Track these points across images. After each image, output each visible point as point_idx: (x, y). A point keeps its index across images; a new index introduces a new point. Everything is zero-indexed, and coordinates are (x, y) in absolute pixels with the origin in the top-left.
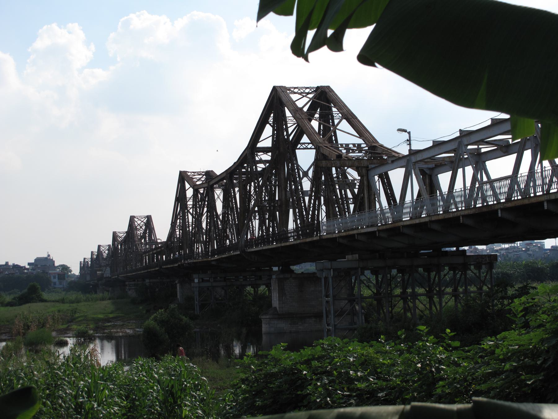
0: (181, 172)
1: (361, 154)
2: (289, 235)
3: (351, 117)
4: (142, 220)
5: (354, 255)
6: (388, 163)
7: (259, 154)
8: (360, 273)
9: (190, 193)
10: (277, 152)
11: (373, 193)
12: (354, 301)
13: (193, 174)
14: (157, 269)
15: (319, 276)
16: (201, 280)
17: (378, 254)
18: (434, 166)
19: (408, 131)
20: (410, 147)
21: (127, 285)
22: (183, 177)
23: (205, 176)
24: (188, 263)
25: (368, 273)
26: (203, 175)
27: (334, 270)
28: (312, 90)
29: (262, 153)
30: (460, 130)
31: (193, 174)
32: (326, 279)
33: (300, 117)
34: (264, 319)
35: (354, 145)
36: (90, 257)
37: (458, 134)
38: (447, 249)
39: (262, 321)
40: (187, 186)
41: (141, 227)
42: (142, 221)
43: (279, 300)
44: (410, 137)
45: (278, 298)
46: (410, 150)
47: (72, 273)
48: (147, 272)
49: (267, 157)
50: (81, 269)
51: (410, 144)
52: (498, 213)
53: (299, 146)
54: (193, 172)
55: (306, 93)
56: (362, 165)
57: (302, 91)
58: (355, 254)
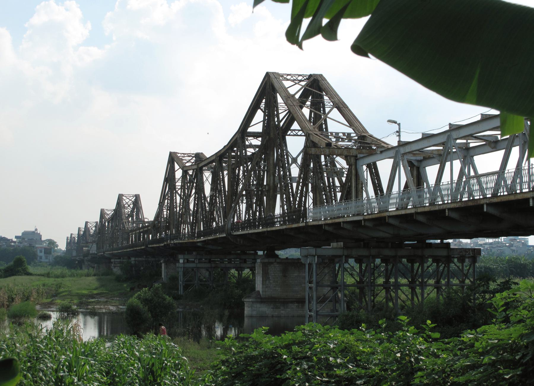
1: (350, 143)
2: (276, 220)
4: (130, 198)
5: (339, 243)
7: (249, 138)
8: (344, 261)
9: (179, 174)
10: (268, 137)
13: (183, 155)
14: (143, 247)
15: (303, 262)
16: (186, 261)
17: (362, 243)
19: (398, 123)
20: (400, 138)
22: (173, 158)
23: (194, 158)
25: (352, 261)
26: (193, 157)
29: (253, 138)
30: (450, 124)
31: (183, 155)
33: (292, 104)
37: (447, 128)
40: (177, 167)
41: (129, 206)
42: (130, 200)
43: (263, 284)
44: (399, 129)
45: (261, 282)
46: (399, 141)
47: (59, 248)
48: (133, 250)
49: (257, 142)
51: (399, 136)
53: (290, 132)
54: (183, 154)
56: (351, 155)
57: (295, 78)
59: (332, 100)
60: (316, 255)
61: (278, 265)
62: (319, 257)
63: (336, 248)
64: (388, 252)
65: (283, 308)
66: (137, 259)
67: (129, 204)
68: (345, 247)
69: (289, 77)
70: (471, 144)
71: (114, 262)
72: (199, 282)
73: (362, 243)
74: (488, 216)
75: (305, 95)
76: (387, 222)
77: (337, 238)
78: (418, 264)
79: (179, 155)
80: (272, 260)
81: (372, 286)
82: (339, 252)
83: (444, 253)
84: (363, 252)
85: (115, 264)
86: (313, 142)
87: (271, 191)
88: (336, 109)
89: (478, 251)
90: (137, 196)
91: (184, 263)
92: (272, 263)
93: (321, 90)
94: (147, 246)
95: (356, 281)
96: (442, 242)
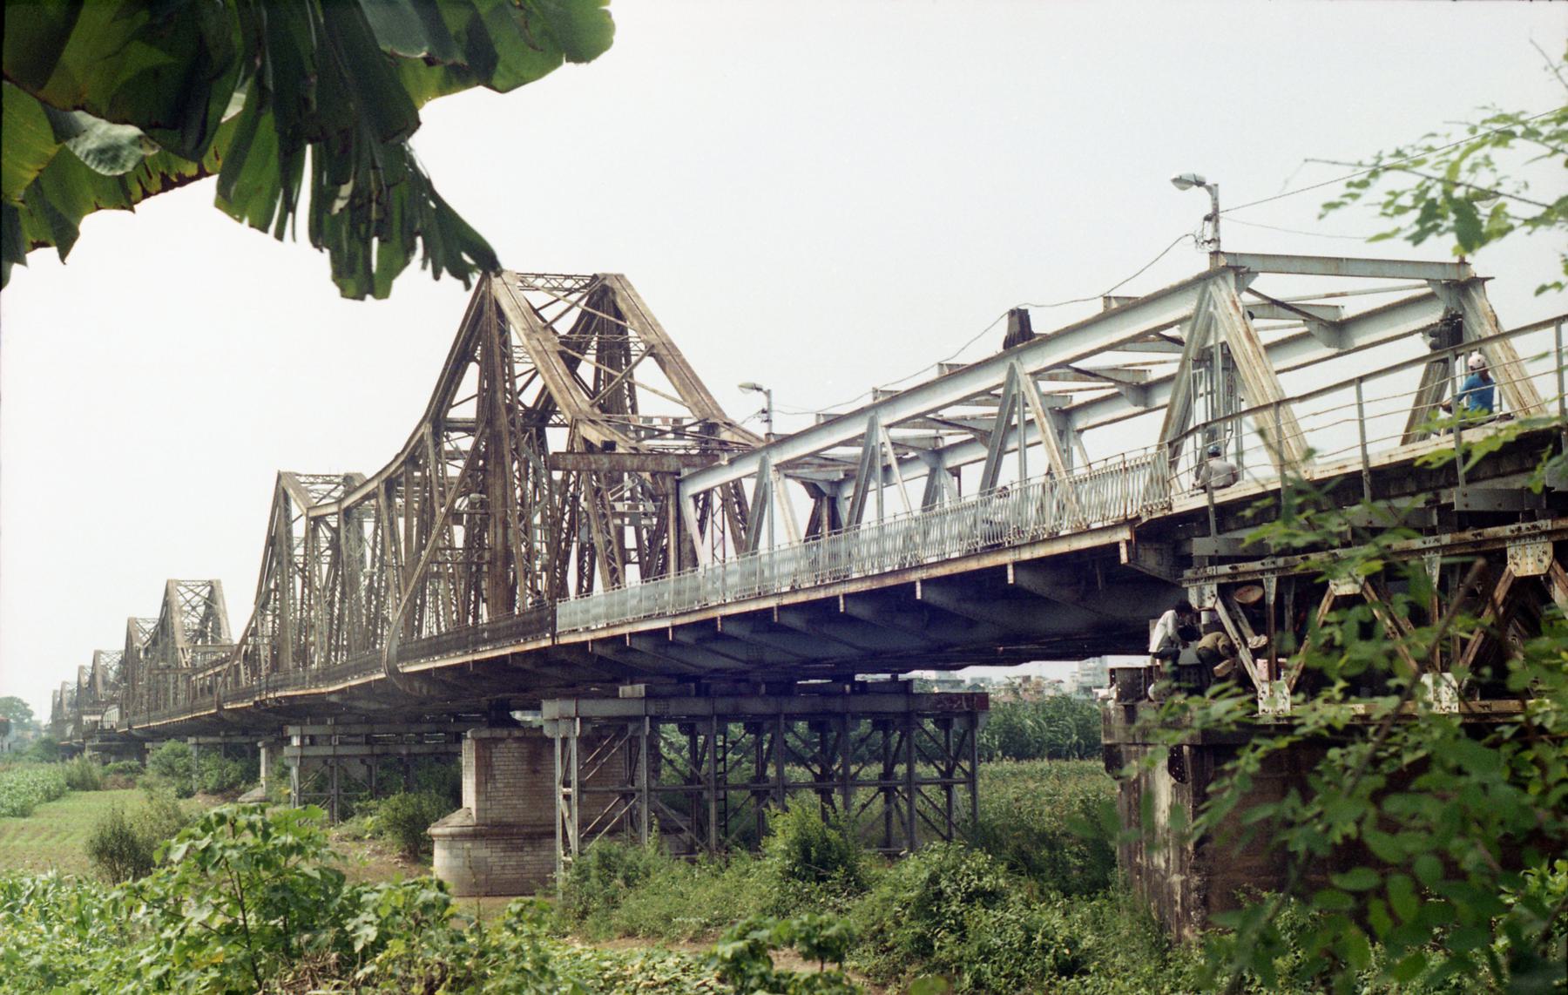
4: (197, 590)
6: (721, 466)
7: (454, 435)
8: (783, 726)
12: (633, 795)
13: (312, 479)
14: (213, 711)
16: (307, 741)
17: (693, 685)
18: (842, 476)
19: (765, 389)
20: (770, 427)
23: (341, 487)
25: (736, 729)
26: (339, 484)
28: (582, 283)
29: (464, 434)
30: (875, 391)
31: (312, 479)
32: (565, 741)
34: (438, 836)
35: (665, 420)
36: (75, 680)
40: (295, 511)
41: (194, 608)
42: (197, 594)
44: (769, 403)
47: (33, 718)
48: (192, 719)
49: (465, 443)
50: (57, 707)
51: (768, 421)
52: (914, 593)
55: (566, 290)
56: (666, 469)
57: (556, 285)
58: (639, 682)
59: (644, 337)
60: (577, 715)
61: (515, 745)
62: (584, 720)
63: (630, 698)
64: (755, 706)
65: (529, 849)
66: (202, 740)
67: (194, 604)
69: (540, 282)
72: (341, 791)
73: (693, 685)
75: (586, 323)
77: (632, 676)
78: (897, 735)
81: (718, 789)
82: (636, 709)
83: (897, 705)
84: (699, 706)
86: (586, 441)
87: (499, 563)
88: (652, 359)
90: (215, 584)
91: (302, 745)
92: (502, 740)
93: (619, 314)
94: (220, 708)
95: (815, 774)
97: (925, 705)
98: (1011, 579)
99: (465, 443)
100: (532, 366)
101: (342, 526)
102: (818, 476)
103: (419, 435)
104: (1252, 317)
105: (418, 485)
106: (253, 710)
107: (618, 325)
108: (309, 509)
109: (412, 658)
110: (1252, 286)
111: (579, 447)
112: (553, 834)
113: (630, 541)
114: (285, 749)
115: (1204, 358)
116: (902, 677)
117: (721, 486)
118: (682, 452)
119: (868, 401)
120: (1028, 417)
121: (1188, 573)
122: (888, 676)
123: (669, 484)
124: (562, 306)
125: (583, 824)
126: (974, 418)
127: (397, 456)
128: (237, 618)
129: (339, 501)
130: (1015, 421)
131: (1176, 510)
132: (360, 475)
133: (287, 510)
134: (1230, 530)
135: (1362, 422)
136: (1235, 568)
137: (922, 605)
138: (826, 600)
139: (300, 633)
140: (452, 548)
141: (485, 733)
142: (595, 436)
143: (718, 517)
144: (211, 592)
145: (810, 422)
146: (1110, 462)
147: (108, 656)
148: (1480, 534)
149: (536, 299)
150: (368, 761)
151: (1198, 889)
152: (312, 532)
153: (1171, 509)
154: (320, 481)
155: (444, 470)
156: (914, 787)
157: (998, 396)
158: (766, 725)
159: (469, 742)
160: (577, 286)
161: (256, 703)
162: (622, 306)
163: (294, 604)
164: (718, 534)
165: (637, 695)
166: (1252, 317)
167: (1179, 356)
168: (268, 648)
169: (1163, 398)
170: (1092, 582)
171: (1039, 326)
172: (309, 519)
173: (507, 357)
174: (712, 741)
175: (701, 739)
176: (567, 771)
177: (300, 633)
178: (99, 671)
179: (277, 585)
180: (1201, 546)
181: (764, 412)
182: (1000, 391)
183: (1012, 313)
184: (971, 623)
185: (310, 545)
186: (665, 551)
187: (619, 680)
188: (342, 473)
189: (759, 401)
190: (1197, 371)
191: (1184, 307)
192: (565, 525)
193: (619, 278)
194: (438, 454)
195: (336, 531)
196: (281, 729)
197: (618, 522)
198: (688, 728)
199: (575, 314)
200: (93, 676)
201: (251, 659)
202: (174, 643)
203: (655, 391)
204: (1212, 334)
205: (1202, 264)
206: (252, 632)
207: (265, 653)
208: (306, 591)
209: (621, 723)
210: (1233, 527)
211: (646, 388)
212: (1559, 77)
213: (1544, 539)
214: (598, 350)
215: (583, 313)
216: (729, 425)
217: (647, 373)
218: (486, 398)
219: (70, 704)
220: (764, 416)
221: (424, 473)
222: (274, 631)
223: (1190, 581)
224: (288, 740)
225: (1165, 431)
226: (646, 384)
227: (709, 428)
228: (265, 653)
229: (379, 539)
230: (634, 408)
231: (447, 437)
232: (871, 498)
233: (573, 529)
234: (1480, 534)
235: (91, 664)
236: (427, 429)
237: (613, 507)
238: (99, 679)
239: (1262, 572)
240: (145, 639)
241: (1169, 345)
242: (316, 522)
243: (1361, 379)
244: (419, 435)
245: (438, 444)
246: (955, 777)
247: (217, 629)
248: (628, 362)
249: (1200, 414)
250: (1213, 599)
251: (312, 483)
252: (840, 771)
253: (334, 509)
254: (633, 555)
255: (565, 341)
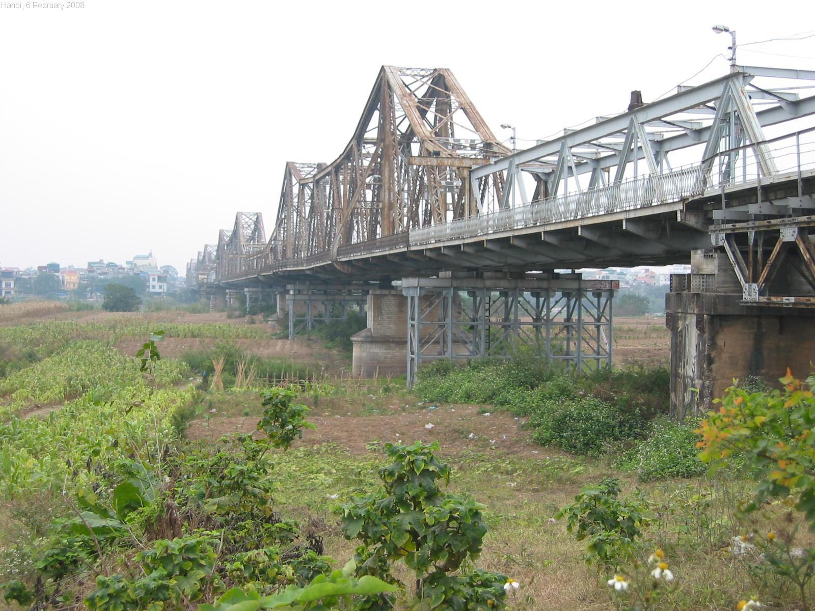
0: (287, 164)
1: (474, 152)
3: (468, 107)
4: (251, 217)
5: (447, 272)
6: (490, 164)
7: (367, 146)
10: (382, 144)
11: (475, 200)
13: (302, 166)
15: (405, 295)
16: (297, 292)
20: (515, 146)
21: (227, 293)
22: (290, 170)
23: (316, 170)
24: (282, 271)
25: (527, 294)
27: (421, 288)
28: (429, 73)
30: (565, 129)
31: (302, 166)
32: (413, 298)
33: (407, 105)
35: (466, 141)
38: (529, 272)
39: (353, 344)
40: (294, 181)
41: (249, 226)
42: (251, 219)
44: (514, 135)
49: (371, 149)
50: (189, 270)
54: (303, 164)
56: (464, 166)
57: (416, 73)
59: (458, 100)
61: (392, 298)
66: (251, 289)
68: (454, 277)
69: (409, 72)
70: (602, 153)
71: (230, 293)
73: (475, 273)
74: (588, 243)
75: (431, 93)
76: (714, 244)
79: (298, 165)
80: (386, 292)
82: (447, 283)
85: (230, 295)
86: (428, 150)
87: (386, 209)
89: (616, 284)
91: (294, 295)
92: (386, 295)
93: (446, 88)
96: (573, 272)
97: (588, 285)
98: (624, 227)
99: (371, 149)
100: (404, 113)
101: (315, 188)
102: (540, 170)
103: (350, 145)
104: (750, 98)
105: (350, 169)
106: (272, 276)
107: (446, 94)
108: (300, 180)
109: (345, 254)
110: (751, 83)
111: (424, 153)
112: (406, 342)
113: (449, 200)
114: (287, 296)
115: (725, 118)
116: (577, 271)
117: (493, 173)
118: (473, 157)
119: (562, 134)
120: (639, 144)
121: (712, 227)
122: (569, 271)
123: (466, 173)
124: (419, 83)
125: (420, 341)
126: (616, 144)
127: (340, 156)
128: (269, 228)
129: (315, 176)
130: (632, 147)
131: (706, 196)
132: (325, 164)
133: (291, 180)
134: (732, 206)
135: (799, 154)
136: (770, 222)
137: (582, 238)
138: (536, 233)
139: (295, 240)
140: (365, 201)
141: (378, 292)
142: (431, 148)
143: (491, 189)
144: (257, 218)
145: (534, 144)
146: (694, 165)
147: (211, 247)
148: (810, 218)
149: (408, 80)
150: (325, 303)
151: (708, 387)
152: (301, 191)
153: (703, 195)
154: (306, 166)
155: (362, 162)
156: (581, 326)
157: (625, 133)
158: (510, 293)
159: (370, 296)
160: (427, 74)
161: (274, 273)
162: (448, 84)
163: (293, 225)
164: (491, 198)
165: (447, 276)
166: (750, 98)
167: (714, 116)
168: (281, 246)
169: (706, 136)
170: (664, 229)
171: (646, 99)
172: (300, 185)
173: (392, 108)
174: (483, 300)
175: (478, 299)
176: (413, 312)
177: (295, 240)
178: (207, 254)
179: (285, 216)
180: (717, 215)
181: (512, 138)
182: (626, 131)
183: (633, 93)
184: (606, 248)
185: (300, 198)
186: (463, 205)
187: (440, 269)
188: (317, 163)
189: (509, 133)
190: (722, 125)
191: (717, 91)
192: (417, 191)
193: (447, 70)
194: (360, 155)
195: (313, 190)
196: (285, 286)
197: (443, 190)
198: (472, 294)
199: (426, 87)
200: (204, 257)
201: (273, 250)
202: (240, 242)
203: (462, 126)
204: (730, 106)
205: (727, 71)
206: (274, 238)
207: (280, 248)
208: (298, 219)
209: (439, 290)
210: (734, 204)
211: (458, 125)
212: (734, 44)
213: (794, 226)
214: (436, 105)
215: (430, 87)
216: (497, 144)
217: (459, 117)
218: (382, 128)
219: (194, 270)
220: (512, 141)
221: (352, 164)
222: (284, 239)
223: (712, 231)
224: (288, 291)
225: (705, 154)
226: (458, 123)
227: (488, 145)
228: (280, 248)
229: (331, 195)
230: (452, 134)
231: (364, 147)
232: (562, 182)
233: (421, 193)
234: (810, 218)
235: (203, 251)
236: (354, 143)
237: (440, 183)
238: (207, 258)
239: (748, 228)
240: (227, 240)
241: (593, 146)
242: (303, 186)
243: (799, 133)
244: (350, 145)
245: (359, 150)
246: (602, 321)
247: (260, 236)
248: (450, 112)
249: (723, 146)
250: (723, 241)
251: (303, 168)
252: (545, 318)
253: (312, 180)
254: (451, 206)
255: (420, 101)
